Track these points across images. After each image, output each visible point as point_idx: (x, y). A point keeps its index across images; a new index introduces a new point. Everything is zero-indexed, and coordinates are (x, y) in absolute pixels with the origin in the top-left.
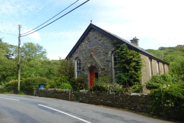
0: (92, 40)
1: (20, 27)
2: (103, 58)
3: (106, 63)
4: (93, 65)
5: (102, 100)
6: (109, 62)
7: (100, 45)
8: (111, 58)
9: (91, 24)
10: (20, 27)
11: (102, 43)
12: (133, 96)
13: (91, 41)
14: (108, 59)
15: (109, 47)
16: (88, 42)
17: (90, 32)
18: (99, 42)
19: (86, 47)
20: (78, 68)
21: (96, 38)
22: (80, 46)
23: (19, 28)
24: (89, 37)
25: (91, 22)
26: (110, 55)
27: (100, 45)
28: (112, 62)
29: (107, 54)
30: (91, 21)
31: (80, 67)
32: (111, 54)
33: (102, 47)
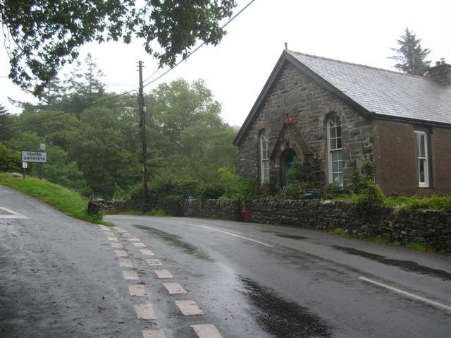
0: (289, 89)
1: (140, 67)
2: (309, 130)
3: (315, 141)
4: (290, 147)
5: (284, 217)
6: (321, 138)
7: (304, 101)
8: (325, 129)
9: (285, 53)
10: (140, 67)
11: (307, 95)
12: (326, 204)
13: (288, 91)
14: (320, 133)
15: (319, 107)
16: (283, 93)
17: (285, 69)
18: (302, 93)
19: (278, 104)
20: (333, 142)
21: (296, 84)
22: (266, 103)
23: (138, 68)
24: (284, 81)
25: (285, 48)
26: (322, 124)
27: (304, 101)
28: (326, 139)
29: (316, 120)
30: (286, 44)
31: (339, 140)
32: (325, 122)
33: (308, 104)
